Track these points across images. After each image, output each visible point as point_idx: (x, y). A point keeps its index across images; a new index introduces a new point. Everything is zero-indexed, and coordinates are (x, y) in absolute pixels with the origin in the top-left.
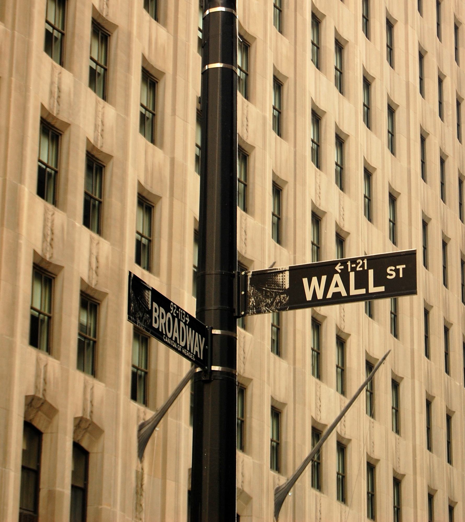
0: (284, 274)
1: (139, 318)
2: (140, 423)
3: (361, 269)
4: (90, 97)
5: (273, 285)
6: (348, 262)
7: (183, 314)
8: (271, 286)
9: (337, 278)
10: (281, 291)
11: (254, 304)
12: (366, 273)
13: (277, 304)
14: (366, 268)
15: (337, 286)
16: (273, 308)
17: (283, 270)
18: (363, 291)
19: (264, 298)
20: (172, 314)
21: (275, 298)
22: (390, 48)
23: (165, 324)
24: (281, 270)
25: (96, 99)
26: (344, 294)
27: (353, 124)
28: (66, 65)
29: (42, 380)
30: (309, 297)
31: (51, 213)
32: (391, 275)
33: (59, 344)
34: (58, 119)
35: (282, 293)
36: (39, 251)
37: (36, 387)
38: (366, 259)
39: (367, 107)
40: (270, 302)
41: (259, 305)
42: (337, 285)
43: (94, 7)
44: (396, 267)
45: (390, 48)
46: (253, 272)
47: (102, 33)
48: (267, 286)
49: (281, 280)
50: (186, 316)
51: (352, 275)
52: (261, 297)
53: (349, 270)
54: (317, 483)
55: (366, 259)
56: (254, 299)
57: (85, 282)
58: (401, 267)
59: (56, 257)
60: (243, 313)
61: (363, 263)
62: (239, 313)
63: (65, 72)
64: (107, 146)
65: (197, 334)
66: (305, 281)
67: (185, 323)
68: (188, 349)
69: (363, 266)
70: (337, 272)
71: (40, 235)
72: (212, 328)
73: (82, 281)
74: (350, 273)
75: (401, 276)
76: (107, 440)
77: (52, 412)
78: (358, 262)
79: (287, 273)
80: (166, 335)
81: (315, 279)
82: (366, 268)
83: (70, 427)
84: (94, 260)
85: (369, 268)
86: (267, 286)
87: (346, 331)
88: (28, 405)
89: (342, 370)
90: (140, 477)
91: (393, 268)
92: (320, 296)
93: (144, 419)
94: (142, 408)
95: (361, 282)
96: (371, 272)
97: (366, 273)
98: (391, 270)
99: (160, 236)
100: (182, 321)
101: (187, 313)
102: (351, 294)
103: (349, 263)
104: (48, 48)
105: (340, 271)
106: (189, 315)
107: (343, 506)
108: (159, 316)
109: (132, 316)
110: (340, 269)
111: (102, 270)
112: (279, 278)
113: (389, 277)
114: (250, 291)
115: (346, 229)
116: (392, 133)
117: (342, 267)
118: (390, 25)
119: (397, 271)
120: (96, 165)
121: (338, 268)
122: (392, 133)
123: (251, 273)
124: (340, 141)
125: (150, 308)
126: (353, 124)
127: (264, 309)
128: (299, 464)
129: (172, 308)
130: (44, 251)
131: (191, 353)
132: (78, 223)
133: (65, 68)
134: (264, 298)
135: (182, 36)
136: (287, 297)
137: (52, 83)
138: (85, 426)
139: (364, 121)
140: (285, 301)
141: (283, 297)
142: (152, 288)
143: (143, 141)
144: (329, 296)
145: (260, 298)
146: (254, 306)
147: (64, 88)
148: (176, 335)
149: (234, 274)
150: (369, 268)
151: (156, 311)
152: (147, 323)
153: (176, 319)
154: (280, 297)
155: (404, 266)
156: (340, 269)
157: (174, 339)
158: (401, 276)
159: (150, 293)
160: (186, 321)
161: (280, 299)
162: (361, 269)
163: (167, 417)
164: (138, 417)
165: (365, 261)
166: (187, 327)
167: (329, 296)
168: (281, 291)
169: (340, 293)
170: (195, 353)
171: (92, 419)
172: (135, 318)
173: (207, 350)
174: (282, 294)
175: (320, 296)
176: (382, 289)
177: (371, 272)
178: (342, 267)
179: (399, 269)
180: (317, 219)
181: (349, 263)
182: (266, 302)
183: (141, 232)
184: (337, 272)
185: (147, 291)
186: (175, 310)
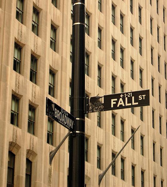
2: (50, 151)
4: (32, 35)
9: (121, 99)
13: (99, 109)
18: (130, 104)
20: (62, 112)
22: (140, 17)
26: (124, 105)
31: (18, 76)
39: (132, 38)
42: (121, 102)
45: (140, 17)
51: (126, 98)
54: (114, 173)
58: (144, 96)
61: (130, 94)
62: (86, 112)
63: (23, 26)
64: (39, 52)
67: (66, 116)
69: (130, 95)
70: (121, 98)
71: (14, 84)
72: (76, 118)
75: (144, 99)
76: (38, 158)
77: (19, 147)
79: (103, 98)
80: (60, 120)
83: (25, 153)
84: (34, 93)
85: (132, 96)
87: (124, 118)
90: (50, 171)
91: (141, 96)
94: (51, 146)
95: (130, 101)
96: (133, 97)
97: (131, 98)
103: (125, 94)
111: (37, 97)
113: (139, 99)
118: (140, 9)
119: (142, 97)
120: (34, 59)
121: (121, 96)
124: (122, 51)
128: (107, 166)
135: (65, 13)
137: (19, 30)
138: (30, 152)
143: (51, 51)
147: (23, 31)
148: (63, 120)
150: (132, 96)
155: (145, 95)
158: (144, 99)
159: (54, 105)
160: (67, 115)
165: (131, 94)
169: (122, 105)
176: (137, 103)
177: (133, 97)
180: (114, 78)
181: (125, 94)
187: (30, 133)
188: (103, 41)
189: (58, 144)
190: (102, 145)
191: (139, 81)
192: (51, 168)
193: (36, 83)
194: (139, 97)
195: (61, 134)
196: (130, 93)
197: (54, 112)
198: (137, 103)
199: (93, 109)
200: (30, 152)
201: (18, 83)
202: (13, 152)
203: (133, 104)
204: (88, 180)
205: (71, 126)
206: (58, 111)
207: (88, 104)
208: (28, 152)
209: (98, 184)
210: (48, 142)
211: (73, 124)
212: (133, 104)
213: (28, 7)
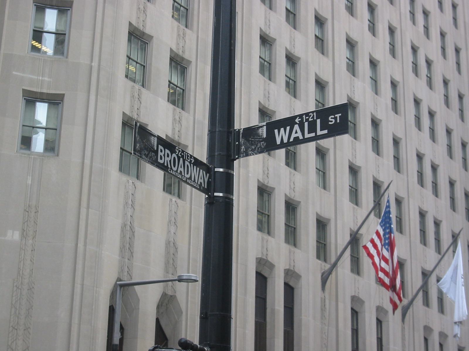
0: (263, 128)
1: (145, 154)
2: (322, 272)
3: (312, 119)
5: (256, 136)
6: (303, 116)
7: (188, 156)
8: (254, 137)
9: (296, 127)
10: (261, 140)
11: (244, 150)
12: (315, 122)
13: (258, 148)
14: (315, 119)
15: (297, 133)
16: (256, 152)
17: (262, 125)
18: (313, 135)
19: (250, 146)
20: (177, 155)
21: (257, 144)
22: (458, 64)
23: (170, 161)
24: (261, 125)
25: (290, 98)
26: (301, 137)
27: (438, 106)
28: (272, 81)
29: (265, 249)
30: (278, 142)
31: (267, 159)
32: (332, 121)
33: (274, 230)
34: (268, 109)
35: (262, 141)
36: (261, 180)
37: (262, 253)
38: (315, 113)
39: (446, 97)
40: (254, 148)
41: (247, 150)
42: (296, 132)
43: (286, 49)
44: (335, 116)
45: (458, 64)
46: (243, 129)
47: (292, 62)
48: (252, 137)
49: (261, 133)
50: (191, 157)
51: (306, 124)
52: (248, 145)
53: (304, 121)
54: (427, 303)
55: (315, 113)
56: (244, 146)
57: (287, 196)
58: (338, 116)
59: (271, 183)
60: (237, 157)
61: (314, 115)
62: (234, 157)
63: (272, 84)
65: (201, 171)
66: (276, 131)
67: (190, 162)
68: (193, 180)
69: (313, 117)
70: (296, 123)
72: (215, 168)
73: (286, 195)
74: (305, 123)
75: (338, 121)
76: (303, 282)
77: (272, 266)
78: (310, 115)
79: (265, 127)
80: (171, 168)
81: (282, 130)
82: (315, 119)
83: (282, 274)
85: (317, 118)
86: (252, 137)
87: (439, 219)
88: (258, 263)
89: (438, 240)
90: (323, 301)
91: (333, 117)
92: (285, 141)
93: (324, 269)
94: (324, 264)
95: (312, 128)
96: (318, 121)
97: (316, 121)
98: (332, 118)
99: (329, 170)
100: (187, 160)
101: (191, 156)
102: (305, 137)
103: (304, 117)
104: (262, 70)
105: (298, 122)
106: (194, 157)
107: (442, 315)
108: (164, 155)
109: (138, 152)
110: (299, 121)
111: (297, 189)
112: (259, 131)
113: (330, 123)
114: (242, 141)
115: (437, 163)
116: (461, 110)
117: (300, 120)
118: (457, 51)
119: (335, 118)
121: (297, 120)
122: (461, 110)
123: (242, 130)
124: (432, 114)
125: (156, 149)
126: (438, 106)
127: (250, 153)
128: (415, 292)
129: (178, 151)
130: (264, 180)
131: (195, 183)
132: (283, 164)
133: (272, 82)
134: (250, 146)
136: (264, 143)
138: (291, 274)
139: (445, 104)
140: (263, 146)
141: (262, 144)
142: (158, 135)
144: (291, 140)
145: (248, 146)
146: (244, 152)
148: (181, 169)
149: (231, 131)
150: (317, 118)
151: (161, 151)
152: (152, 159)
153: (181, 159)
154: (260, 144)
155: (340, 115)
156: (299, 121)
157: (179, 172)
158: (338, 121)
159: (156, 139)
160: (191, 161)
161: (261, 145)
162: (312, 119)
163: (337, 268)
164: (321, 268)
165: (315, 114)
166: (192, 165)
167: (291, 140)
168: (261, 140)
170: (199, 183)
171: (294, 270)
172: (140, 154)
173: (210, 182)
174: (262, 142)
175: (285, 141)
176: (325, 132)
177: (318, 121)
178: (300, 120)
179: (337, 117)
180: (420, 157)
181: (304, 117)
182: (251, 148)
183: (319, 168)
184: (296, 123)
185: (153, 137)
186: (180, 153)
187: (289, 244)
188: (400, 102)
189: (333, 260)
190: (405, 260)
191: (461, 160)
192: (324, 296)
193: (295, 169)
194: (330, 119)
195: (338, 245)
196: (313, 112)
197: (156, 152)
198: (325, 132)
199: (247, 149)
200: (289, 273)
201: (266, 169)
202: (263, 273)
203: (318, 134)
204: (386, 315)
205: (201, 183)
206: (167, 151)
207: (239, 142)
208: (287, 273)
209: (401, 320)
210: (318, 257)
211: (208, 180)
212: (318, 134)
213: (277, 55)
